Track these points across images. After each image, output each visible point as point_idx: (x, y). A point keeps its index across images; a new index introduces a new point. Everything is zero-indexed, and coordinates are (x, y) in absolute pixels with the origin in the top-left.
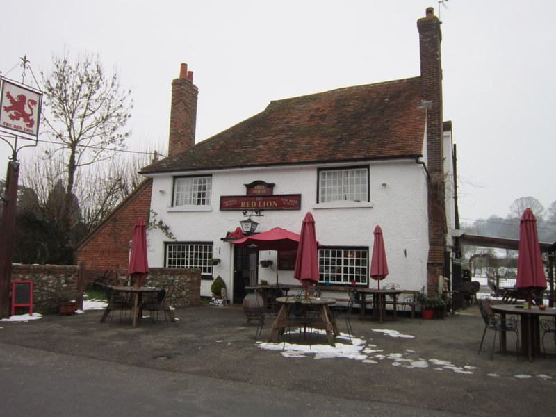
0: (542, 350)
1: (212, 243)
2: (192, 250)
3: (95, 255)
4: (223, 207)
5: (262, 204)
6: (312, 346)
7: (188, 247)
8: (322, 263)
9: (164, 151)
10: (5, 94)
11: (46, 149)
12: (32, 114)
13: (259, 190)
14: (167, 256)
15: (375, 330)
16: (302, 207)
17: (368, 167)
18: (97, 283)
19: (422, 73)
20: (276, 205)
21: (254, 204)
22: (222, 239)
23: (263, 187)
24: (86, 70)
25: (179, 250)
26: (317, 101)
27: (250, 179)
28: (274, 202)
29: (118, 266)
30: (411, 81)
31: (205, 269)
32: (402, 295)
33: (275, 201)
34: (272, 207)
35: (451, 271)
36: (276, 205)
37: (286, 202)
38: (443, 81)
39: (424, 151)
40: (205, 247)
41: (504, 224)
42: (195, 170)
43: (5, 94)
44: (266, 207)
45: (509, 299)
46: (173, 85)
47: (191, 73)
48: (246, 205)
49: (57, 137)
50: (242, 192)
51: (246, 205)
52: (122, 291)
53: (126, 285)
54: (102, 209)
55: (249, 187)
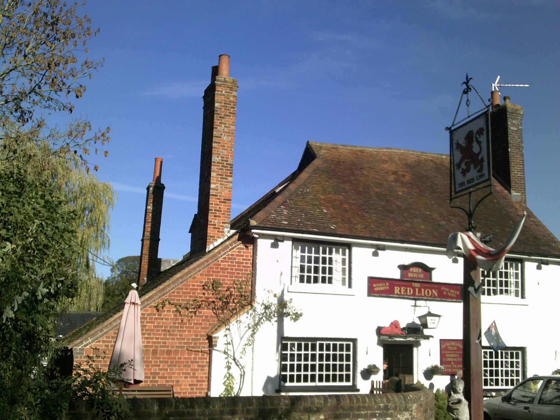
0: (461, 260)
1: (354, 341)
2: (306, 349)
3: (34, 192)
4: (371, 292)
5: (420, 291)
6: (482, 301)
7: (506, 354)
8: (486, 365)
9: (415, 349)
10: (455, 146)
11: (37, 126)
12: (480, 153)
13: (415, 273)
14: (463, 187)
15: (491, 249)
16: (355, 337)
17: (521, 261)
18: (386, 388)
19: (198, 212)
20: (436, 295)
21: (410, 291)
22: (432, 337)
23: (420, 270)
24: (50, 279)
25: (512, 357)
26: (229, 388)
27: (409, 258)
28: (434, 291)
29: (213, 294)
30: (192, 235)
31: (341, 377)
32: (514, 392)
33: (435, 289)
34: (431, 296)
35: (523, 85)
36: (436, 295)
37: (447, 292)
38: (203, 106)
39: (164, 349)
40: (335, 346)
41: (61, 186)
42: (303, 232)
43: (455, 146)
44: (425, 296)
45: (119, 267)
46: (394, 321)
47: (190, 232)
48: (400, 291)
49: (73, 36)
50: (396, 274)
51: (400, 291)
52: (447, 353)
53: (497, 384)
54: (51, 368)
55: (403, 268)
